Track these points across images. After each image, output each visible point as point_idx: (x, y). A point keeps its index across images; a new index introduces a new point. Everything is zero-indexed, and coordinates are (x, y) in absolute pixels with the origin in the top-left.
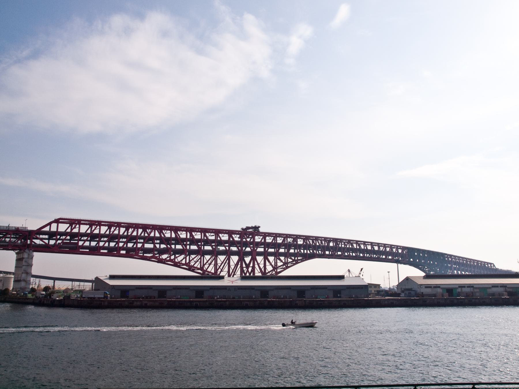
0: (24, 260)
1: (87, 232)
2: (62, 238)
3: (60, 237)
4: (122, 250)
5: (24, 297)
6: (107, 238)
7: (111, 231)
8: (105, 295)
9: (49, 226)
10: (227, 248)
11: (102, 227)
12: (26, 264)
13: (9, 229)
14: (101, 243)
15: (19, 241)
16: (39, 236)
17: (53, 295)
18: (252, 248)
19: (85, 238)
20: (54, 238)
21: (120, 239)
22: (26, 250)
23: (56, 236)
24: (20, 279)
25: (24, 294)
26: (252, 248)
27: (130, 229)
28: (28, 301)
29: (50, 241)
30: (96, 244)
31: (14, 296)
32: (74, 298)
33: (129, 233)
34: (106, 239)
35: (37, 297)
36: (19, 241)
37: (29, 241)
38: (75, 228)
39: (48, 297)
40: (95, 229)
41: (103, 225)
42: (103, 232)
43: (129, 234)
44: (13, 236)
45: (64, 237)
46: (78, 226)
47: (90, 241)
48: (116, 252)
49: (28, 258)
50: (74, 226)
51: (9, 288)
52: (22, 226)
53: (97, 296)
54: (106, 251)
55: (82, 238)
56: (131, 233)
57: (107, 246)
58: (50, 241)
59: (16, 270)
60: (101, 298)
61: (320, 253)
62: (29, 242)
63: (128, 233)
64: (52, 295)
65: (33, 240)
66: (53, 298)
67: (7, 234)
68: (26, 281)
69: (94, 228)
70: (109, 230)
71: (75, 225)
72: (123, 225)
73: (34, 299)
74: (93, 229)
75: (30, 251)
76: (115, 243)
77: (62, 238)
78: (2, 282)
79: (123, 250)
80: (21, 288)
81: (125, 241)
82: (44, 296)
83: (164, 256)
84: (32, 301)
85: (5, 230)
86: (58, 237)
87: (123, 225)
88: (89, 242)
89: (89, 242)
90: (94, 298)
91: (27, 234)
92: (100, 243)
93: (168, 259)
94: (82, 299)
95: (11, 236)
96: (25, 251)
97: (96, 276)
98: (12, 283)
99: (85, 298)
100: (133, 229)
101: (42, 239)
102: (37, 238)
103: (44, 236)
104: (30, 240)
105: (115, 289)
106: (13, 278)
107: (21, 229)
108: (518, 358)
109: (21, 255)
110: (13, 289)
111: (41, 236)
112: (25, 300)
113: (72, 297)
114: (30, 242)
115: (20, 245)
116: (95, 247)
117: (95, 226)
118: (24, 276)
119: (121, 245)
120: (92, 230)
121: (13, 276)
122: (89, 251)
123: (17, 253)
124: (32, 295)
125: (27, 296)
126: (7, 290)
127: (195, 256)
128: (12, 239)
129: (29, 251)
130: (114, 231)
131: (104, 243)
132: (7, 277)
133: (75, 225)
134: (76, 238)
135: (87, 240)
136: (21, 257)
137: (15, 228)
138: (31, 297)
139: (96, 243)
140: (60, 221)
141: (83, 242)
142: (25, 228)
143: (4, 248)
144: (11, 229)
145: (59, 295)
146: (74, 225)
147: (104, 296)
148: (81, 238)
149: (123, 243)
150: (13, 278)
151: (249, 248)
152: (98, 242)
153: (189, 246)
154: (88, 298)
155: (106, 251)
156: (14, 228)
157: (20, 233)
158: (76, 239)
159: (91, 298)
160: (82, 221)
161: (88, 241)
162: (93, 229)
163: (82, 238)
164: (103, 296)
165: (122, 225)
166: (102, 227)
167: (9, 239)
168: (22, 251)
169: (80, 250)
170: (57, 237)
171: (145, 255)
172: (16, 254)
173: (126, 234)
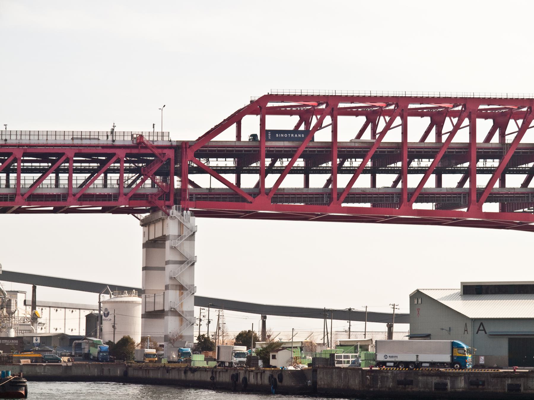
0: (168, 244)
2: (278, 164)
3: (274, 162)
4: (486, 202)
5: (183, 366)
6: (432, 160)
7: (443, 131)
8: (457, 353)
9: (234, 126)
11: (341, 119)
12: (178, 258)
13: (113, 141)
14: (410, 177)
15: (149, 182)
16: (208, 161)
17: (274, 357)
19: (357, 163)
20: (254, 165)
21: (478, 161)
22: (171, 211)
23: (257, 157)
24: (161, 308)
25: (181, 354)
27: (512, 122)
28: (197, 376)
29: (243, 176)
30: (396, 183)
31: (150, 361)
32: (346, 365)
33: (507, 137)
34: (426, 163)
35: (223, 363)
36: (149, 182)
37: (176, 179)
38: (321, 128)
39: (260, 363)
40: (388, 127)
41: (416, 113)
42: (414, 137)
43: (509, 139)
44: (127, 165)
45: (286, 162)
46: (328, 120)
47: (373, 172)
48: (465, 210)
49: (179, 236)
50: (314, 121)
51: (131, 337)
52: (151, 130)
53: (426, 358)
54: (429, 206)
55: (347, 164)
56: (516, 134)
57: (431, 189)
58: (378, 176)
59: (146, 280)
60: (442, 364)
62: (177, 183)
63: (503, 136)
64: (271, 354)
65: (191, 177)
66: (275, 367)
67: (110, 157)
68: (180, 315)
69: (384, 125)
70: (434, 128)
71: (319, 117)
72: (486, 107)
73: (213, 370)
74: (380, 129)
75: (185, 212)
76: (459, 177)
77: (278, 164)
78: (109, 317)
79: (491, 199)
80: (166, 338)
81: (498, 168)
82: (245, 360)
84: (207, 377)
85: (104, 147)
86: (268, 162)
87: (486, 107)
88: (368, 176)
89: (369, 176)
90: (418, 365)
91: (170, 154)
92: (409, 176)
94: (377, 368)
95: (122, 166)
96: (168, 215)
98: (139, 321)
99: (384, 363)
100: (520, 122)
101: (216, 172)
102: (201, 170)
103: (221, 162)
104: (179, 175)
105: (486, 333)
106: (139, 304)
107: (151, 139)
109: (159, 225)
110: (144, 339)
111: (213, 162)
112: (185, 372)
113: (340, 362)
114: (180, 183)
115: (152, 195)
116: (392, 194)
117: (388, 118)
118: (172, 296)
119: (482, 181)
120: (377, 132)
121: (139, 300)
122: (374, 206)
123: (145, 223)
124: (207, 359)
125: (190, 361)
126: (126, 341)
128: (125, 175)
129: (180, 214)
130: (452, 134)
132: (121, 302)
133: (319, 117)
134: (326, 162)
135: (362, 170)
136: (159, 234)
137: (132, 135)
138: (204, 364)
139: (394, 177)
140: (270, 105)
141: (351, 176)
142: (163, 136)
143: (108, 204)
144: (120, 141)
145: (294, 355)
146: (314, 117)
147: (452, 357)
148: (342, 163)
149: (490, 176)
150: (139, 304)
151: (270, 176)
152: (402, 174)
154: (397, 364)
155: (429, 206)
156: (130, 138)
157: (148, 151)
158: (324, 165)
159: (406, 364)
160: (484, 104)
161: (365, 172)
162: (380, 129)
163: (347, 164)
164: (446, 358)
165: (481, 107)
166: (341, 119)
167: (118, 175)
168: (160, 214)
169: (343, 205)
170: (263, 163)
172: (142, 225)
173: (496, 139)
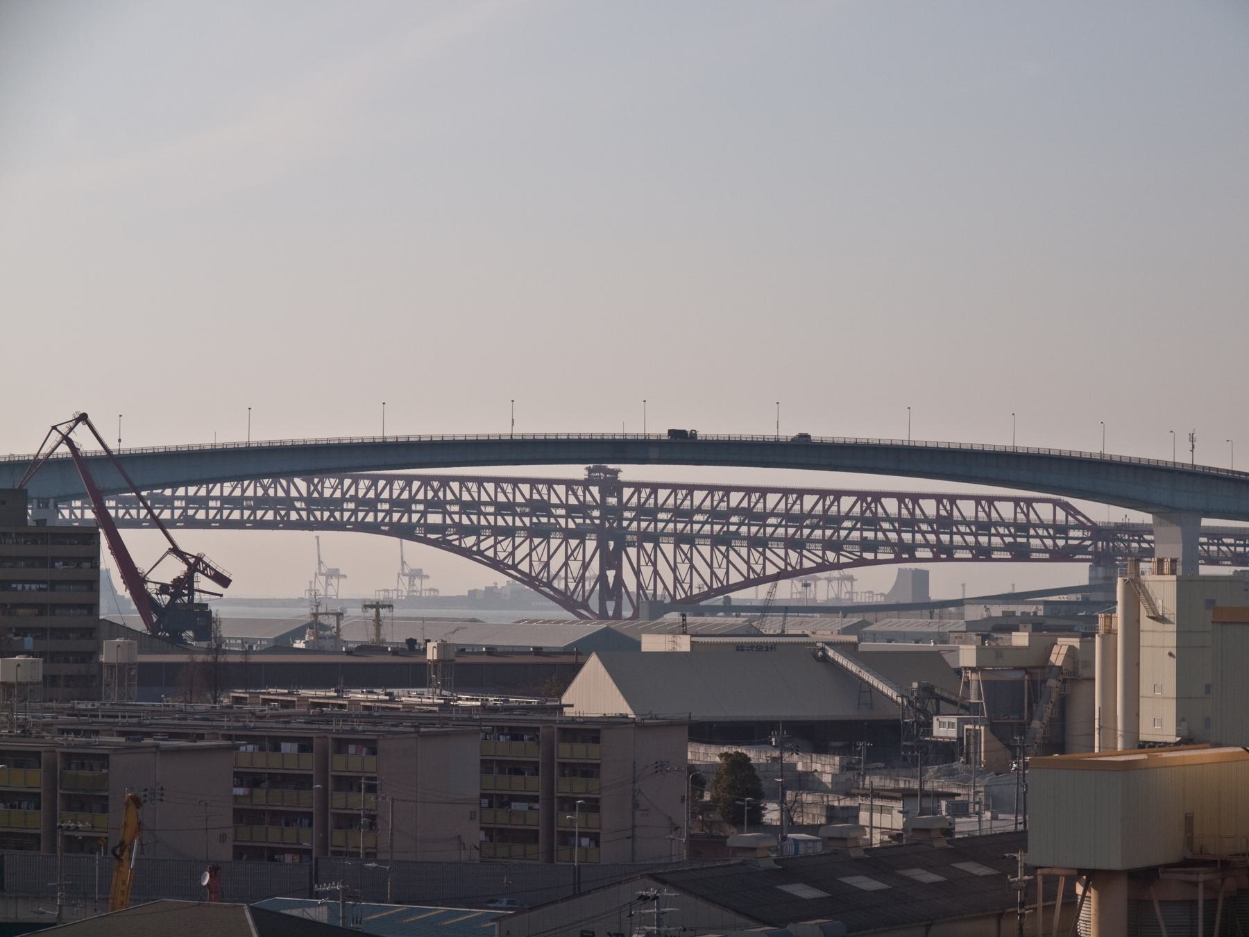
1: (401, 498)
10: (304, 514)
18: (916, 529)
26: (916, 529)
61: (305, 518)
83: (469, 541)
93: (475, 549)
97: (337, 567)
108: (4, 585)
127: (541, 539)
131: (700, 525)
135: (779, 525)
153: (864, 532)
171: (429, 536)
